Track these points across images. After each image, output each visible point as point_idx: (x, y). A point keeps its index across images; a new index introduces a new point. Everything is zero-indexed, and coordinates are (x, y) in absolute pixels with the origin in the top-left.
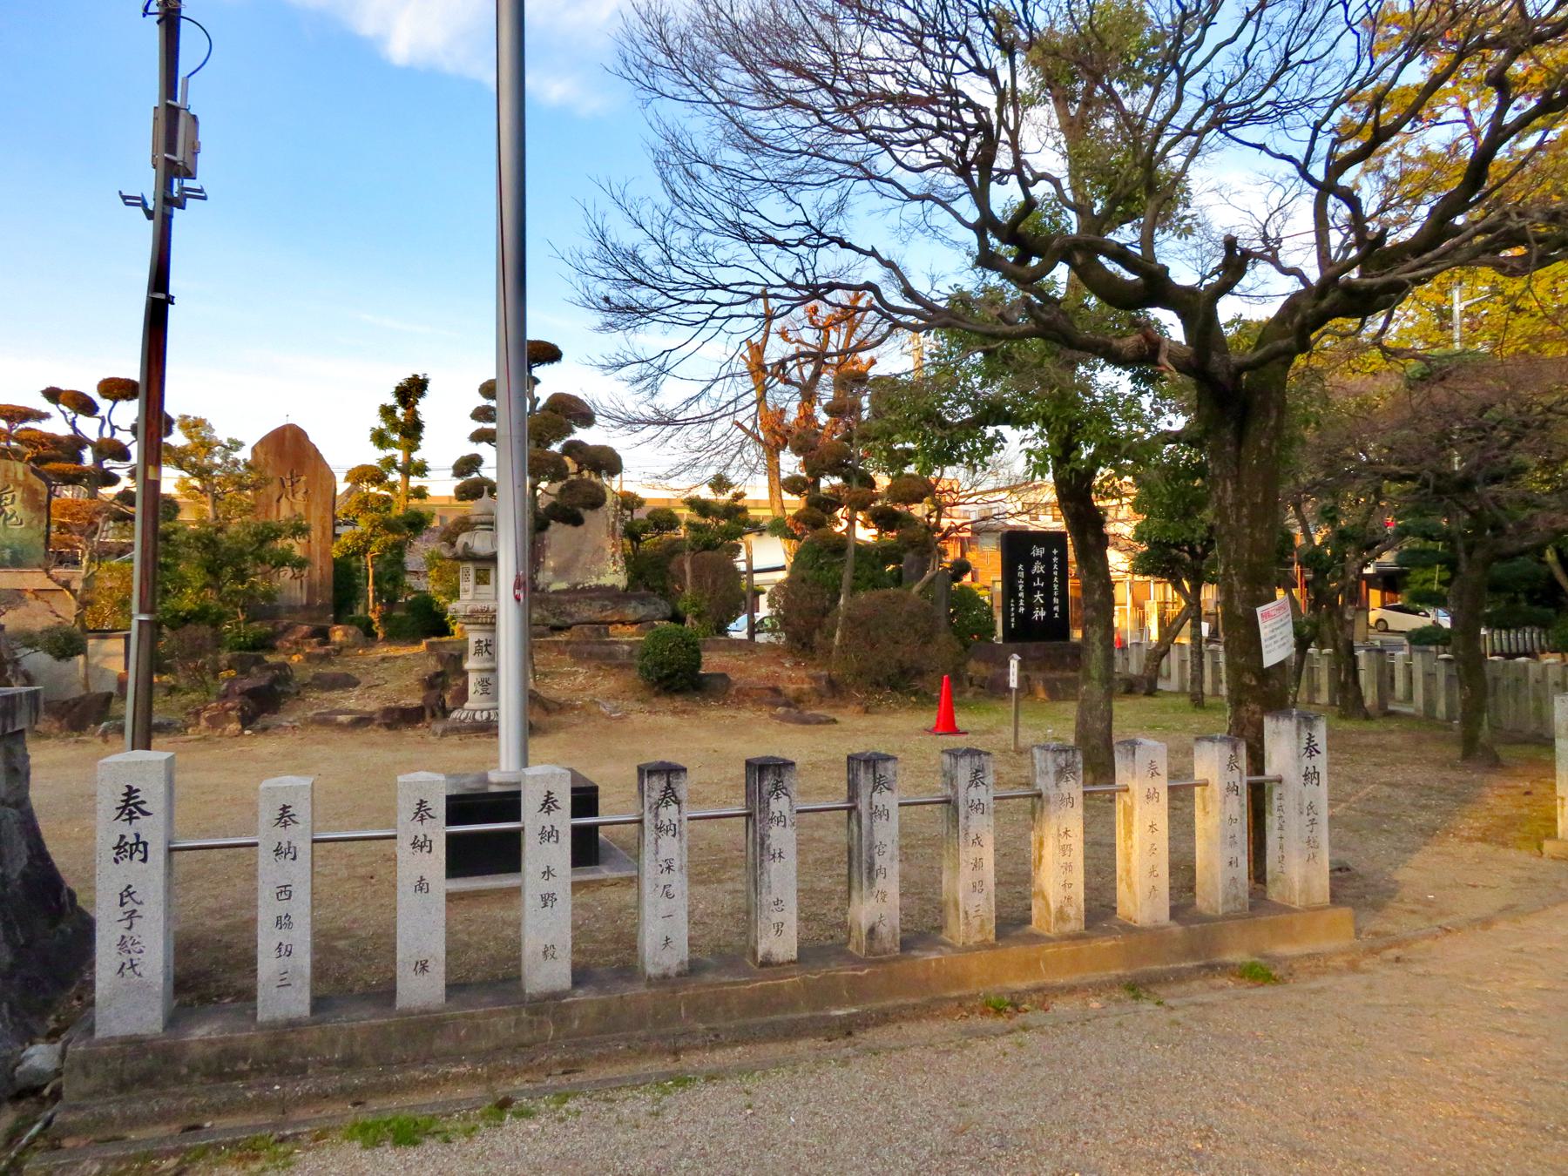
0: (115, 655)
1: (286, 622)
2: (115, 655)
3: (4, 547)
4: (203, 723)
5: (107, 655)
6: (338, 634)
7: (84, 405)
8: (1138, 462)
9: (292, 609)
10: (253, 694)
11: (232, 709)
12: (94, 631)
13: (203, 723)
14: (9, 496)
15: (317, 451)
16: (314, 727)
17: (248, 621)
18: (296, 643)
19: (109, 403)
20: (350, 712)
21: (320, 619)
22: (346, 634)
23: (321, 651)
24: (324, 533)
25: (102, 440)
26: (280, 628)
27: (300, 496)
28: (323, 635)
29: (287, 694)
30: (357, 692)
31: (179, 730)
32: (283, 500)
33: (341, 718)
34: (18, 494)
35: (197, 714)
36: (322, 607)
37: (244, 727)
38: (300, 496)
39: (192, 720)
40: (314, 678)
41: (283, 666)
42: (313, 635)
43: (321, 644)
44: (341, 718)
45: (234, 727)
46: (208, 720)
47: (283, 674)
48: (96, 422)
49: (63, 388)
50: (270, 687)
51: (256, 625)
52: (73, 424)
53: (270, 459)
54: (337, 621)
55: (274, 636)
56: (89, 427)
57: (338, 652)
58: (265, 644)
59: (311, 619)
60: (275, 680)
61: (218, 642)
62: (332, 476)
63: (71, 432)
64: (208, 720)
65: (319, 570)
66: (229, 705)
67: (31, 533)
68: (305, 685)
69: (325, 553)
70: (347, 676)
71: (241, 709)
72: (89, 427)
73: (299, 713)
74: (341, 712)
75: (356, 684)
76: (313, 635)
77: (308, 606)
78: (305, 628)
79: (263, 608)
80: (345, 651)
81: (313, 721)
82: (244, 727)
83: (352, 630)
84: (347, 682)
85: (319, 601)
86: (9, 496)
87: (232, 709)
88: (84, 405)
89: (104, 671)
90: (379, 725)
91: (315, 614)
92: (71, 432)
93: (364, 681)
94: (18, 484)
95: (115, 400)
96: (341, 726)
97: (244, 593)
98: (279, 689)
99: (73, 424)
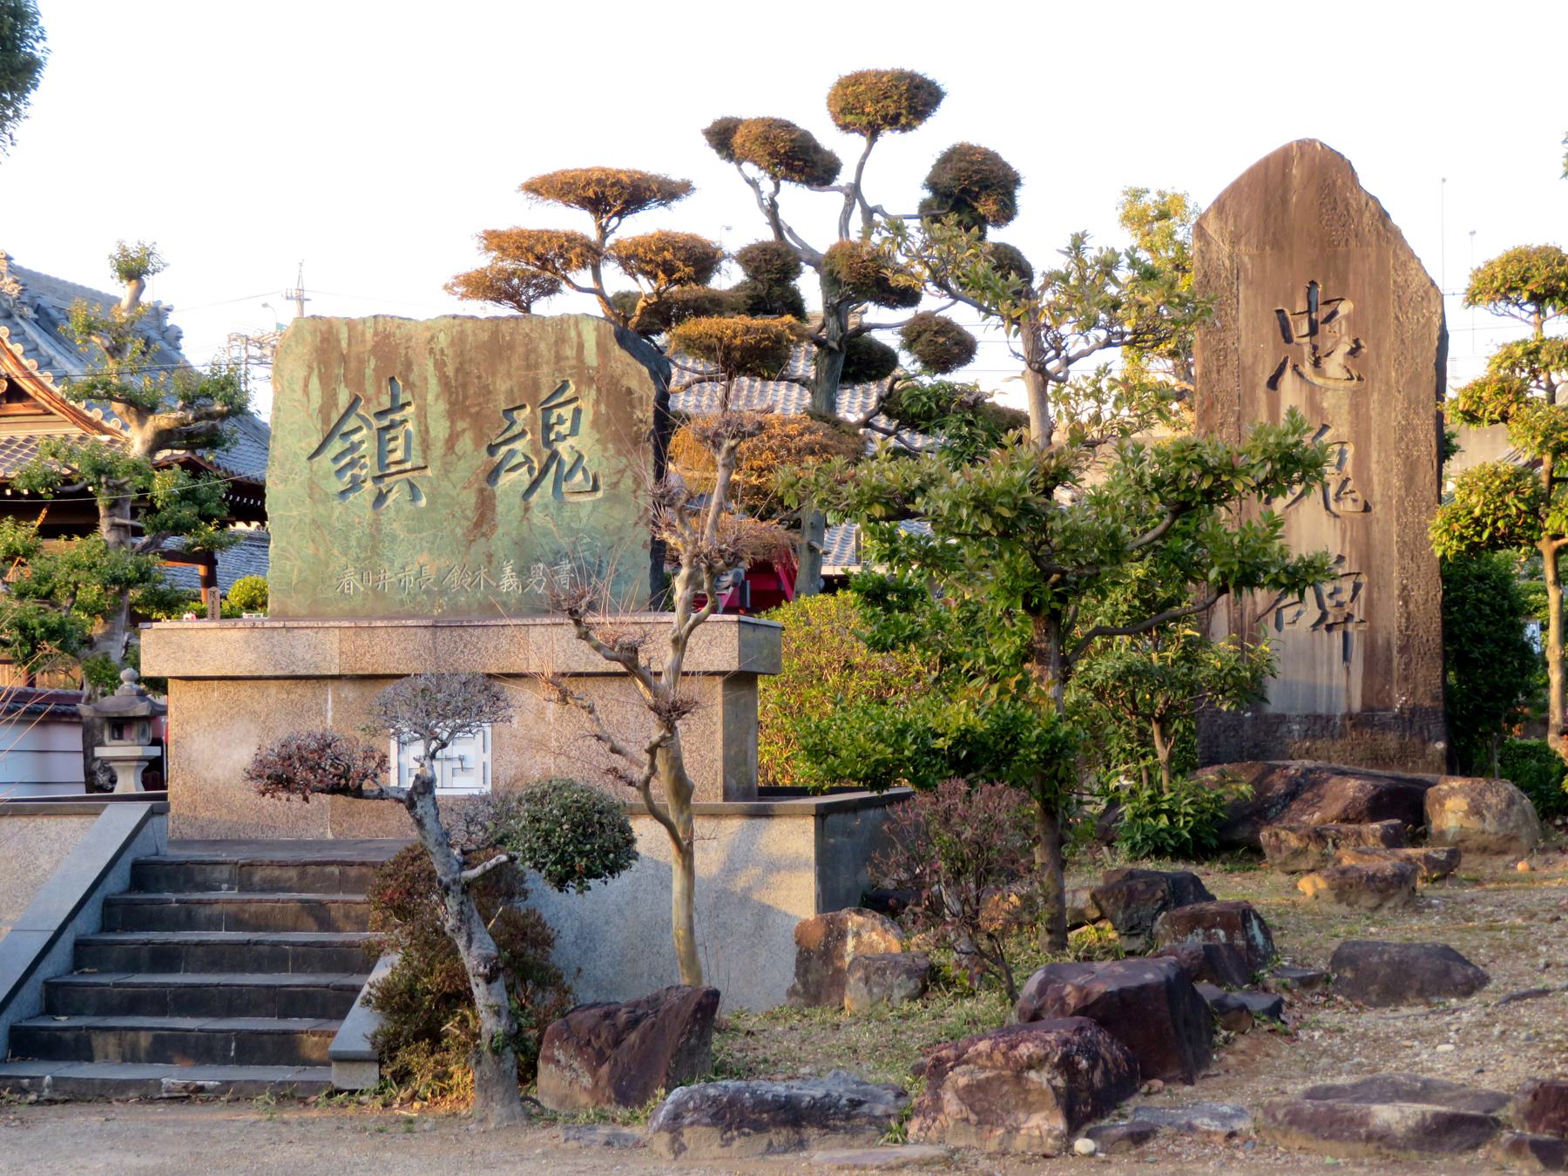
0: (793, 866)
1: (1295, 766)
2: (793, 866)
3: (7, 486)
4: (951, 1104)
5: (773, 866)
6: (1453, 807)
7: (801, 161)
8: (1546, 1047)
9: (1319, 725)
10: (1113, 1012)
11: (1033, 1064)
12: (631, 784)
13: (951, 1104)
14: (567, 412)
15: (1384, 216)
16: (1297, 1139)
17: (1183, 765)
18: (1319, 836)
19: (858, 142)
20: (1425, 1092)
21: (1403, 756)
22: (1476, 810)
23: (1386, 863)
24: (1409, 481)
25: (846, 251)
26: (1279, 786)
27: (1335, 365)
28: (1404, 809)
29: (1238, 1016)
30: (1469, 1012)
31: (880, 1123)
32: (1288, 377)
33: (1388, 1115)
34: (586, 405)
35: (937, 1072)
36: (1410, 719)
37: (1075, 1124)
38: (1335, 365)
39: (919, 1092)
40: (1338, 960)
41: (1242, 916)
42: (1376, 808)
43: (1392, 840)
44: (1388, 1115)
45: (1044, 1123)
46: (969, 1094)
47: (1241, 950)
48: (828, 202)
49: (744, 117)
50: (1181, 983)
51: (1209, 775)
52: (772, 211)
53: (1246, 253)
54: (1460, 763)
55: (1259, 811)
56: (814, 219)
57: (1445, 870)
58: (1229, 836)
59: (1377, 759)
60: (1210, 964)
61: (1057, 825)
62: (1431, 290)
63: (768, 235)
64: (969, 1094)
65: (1406, 601)
66: (1025, 1050)
67: (618, 513)
68: (1307, 983)
69: (1414, 544)
70: (1447, 953)
71: (1066, 1065)
72: (814, 219)
73: (1263, 1084)
74: (1396, 1092)
75: (1474, 983)
76: (1376, 808)
77: (1366, 719)
78: (1351, 787)
79: (1227, 722)
80: (1470, 864)
81: (1295, 1118)
82: (1075, 1124)
83: (1499, 792)
84: (1445, 977)
85: (1399, 701)
86: (567, 412)
87: (1033, 1064)
88: (801, 161)
89: (765, 911)
90: (1516, 1147)
91: (1391, 741)
92: (768, 235)
93: (1499, 981)
94: (585, 377)
95: (873, 132)
96: (1382, 1140)
97: (1163, 678)
98: (1207, 990)
99: (772, 211)
